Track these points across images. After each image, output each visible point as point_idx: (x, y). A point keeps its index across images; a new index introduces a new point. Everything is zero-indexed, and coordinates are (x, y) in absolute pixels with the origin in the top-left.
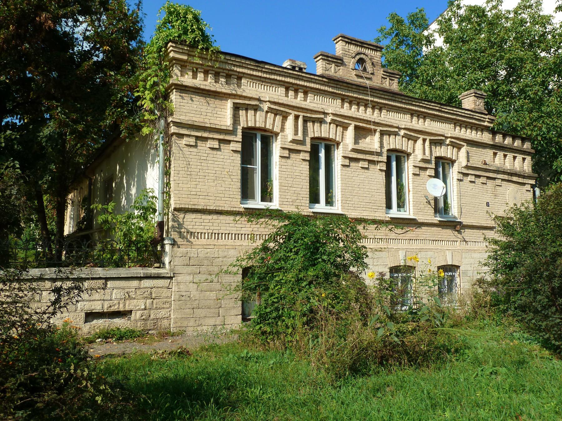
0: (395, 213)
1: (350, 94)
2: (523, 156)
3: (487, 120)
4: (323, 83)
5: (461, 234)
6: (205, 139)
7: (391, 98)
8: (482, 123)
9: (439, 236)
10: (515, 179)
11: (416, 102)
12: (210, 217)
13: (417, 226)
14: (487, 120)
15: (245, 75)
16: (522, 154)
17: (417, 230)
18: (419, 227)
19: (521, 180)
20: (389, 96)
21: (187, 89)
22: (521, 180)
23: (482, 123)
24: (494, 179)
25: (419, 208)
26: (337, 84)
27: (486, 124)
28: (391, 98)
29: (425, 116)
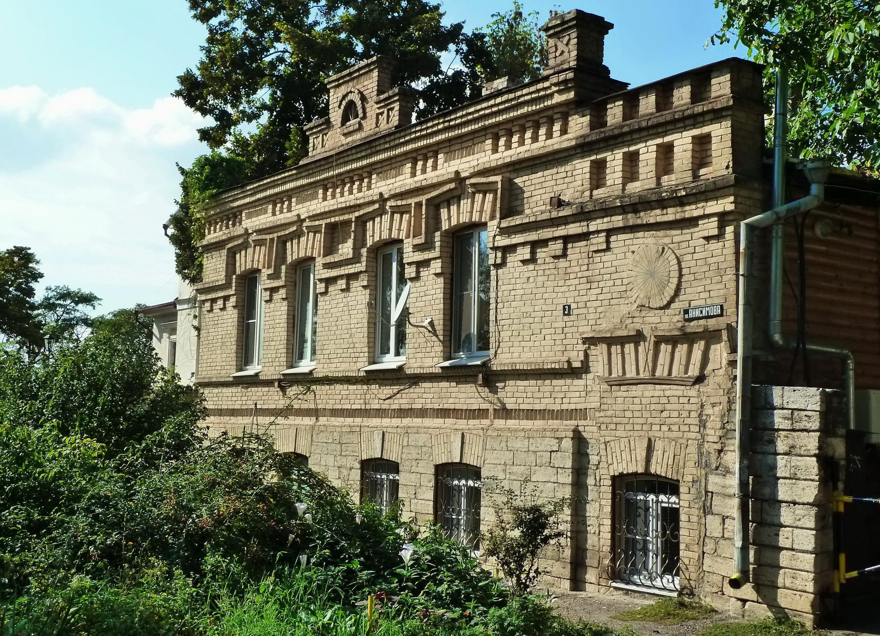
0: (390, 362)
1: (342, 170)
2: (696, 132)
3: (554, 89)
4: (295, 177)
5: (496, 392)
6: (544, 243)
7: (369, 151)
8: (549, 103)
9: (451, 401)
10: (655, 216)
11: (405, 136)
12: (216, 391)
13: (412, 381)
14: (554, 89)
15: (440, 146)
16: (685, 128)
17: (411, 390)
18: (416, 384)
19: (671, 214)
20: (366, 150)
21: (557, 156)
22: (671, 214)
23: (549, 103)
24: (584, 236)
25: (416, 345)
26: (308, 170)
27: (558, 99)
28: (369, 151)
29: (430, 153)
